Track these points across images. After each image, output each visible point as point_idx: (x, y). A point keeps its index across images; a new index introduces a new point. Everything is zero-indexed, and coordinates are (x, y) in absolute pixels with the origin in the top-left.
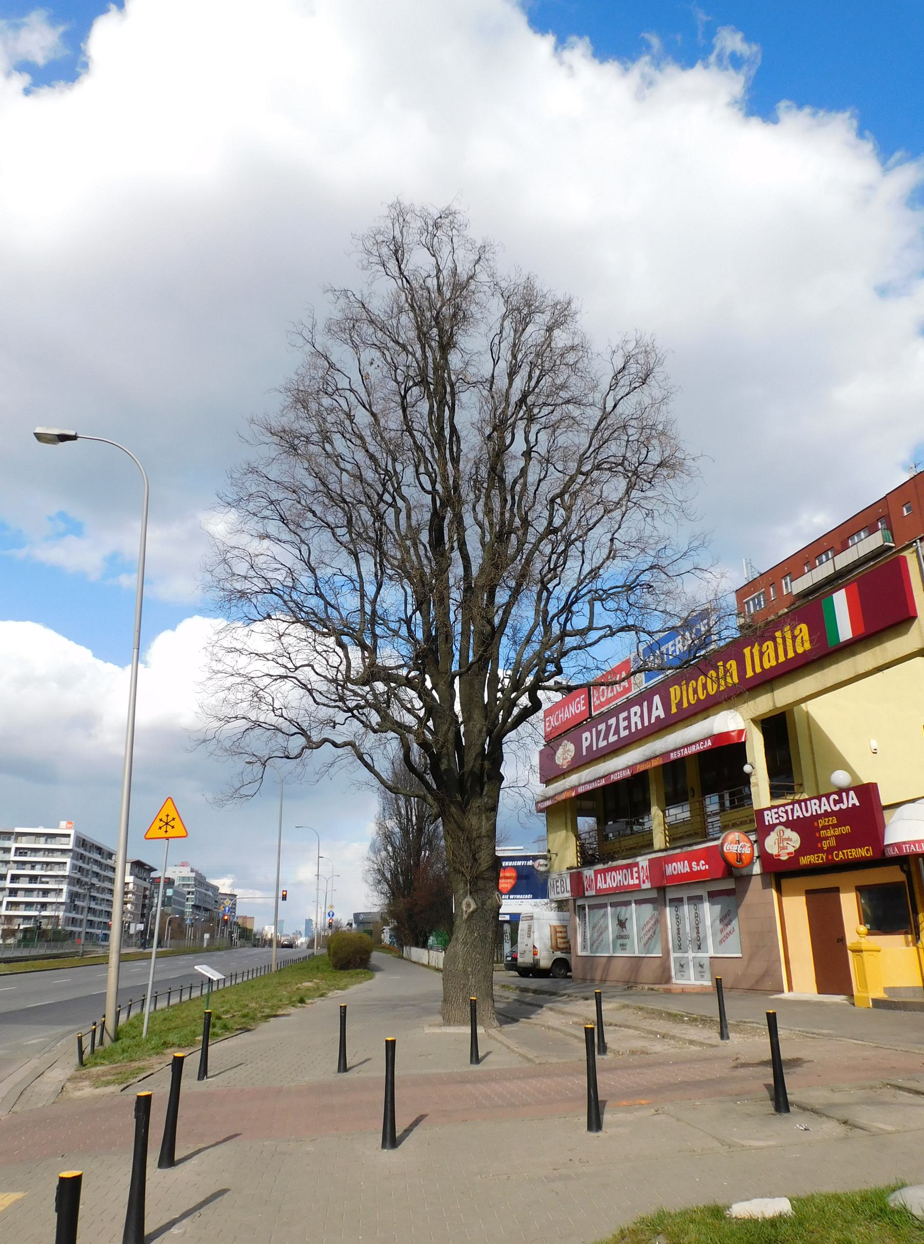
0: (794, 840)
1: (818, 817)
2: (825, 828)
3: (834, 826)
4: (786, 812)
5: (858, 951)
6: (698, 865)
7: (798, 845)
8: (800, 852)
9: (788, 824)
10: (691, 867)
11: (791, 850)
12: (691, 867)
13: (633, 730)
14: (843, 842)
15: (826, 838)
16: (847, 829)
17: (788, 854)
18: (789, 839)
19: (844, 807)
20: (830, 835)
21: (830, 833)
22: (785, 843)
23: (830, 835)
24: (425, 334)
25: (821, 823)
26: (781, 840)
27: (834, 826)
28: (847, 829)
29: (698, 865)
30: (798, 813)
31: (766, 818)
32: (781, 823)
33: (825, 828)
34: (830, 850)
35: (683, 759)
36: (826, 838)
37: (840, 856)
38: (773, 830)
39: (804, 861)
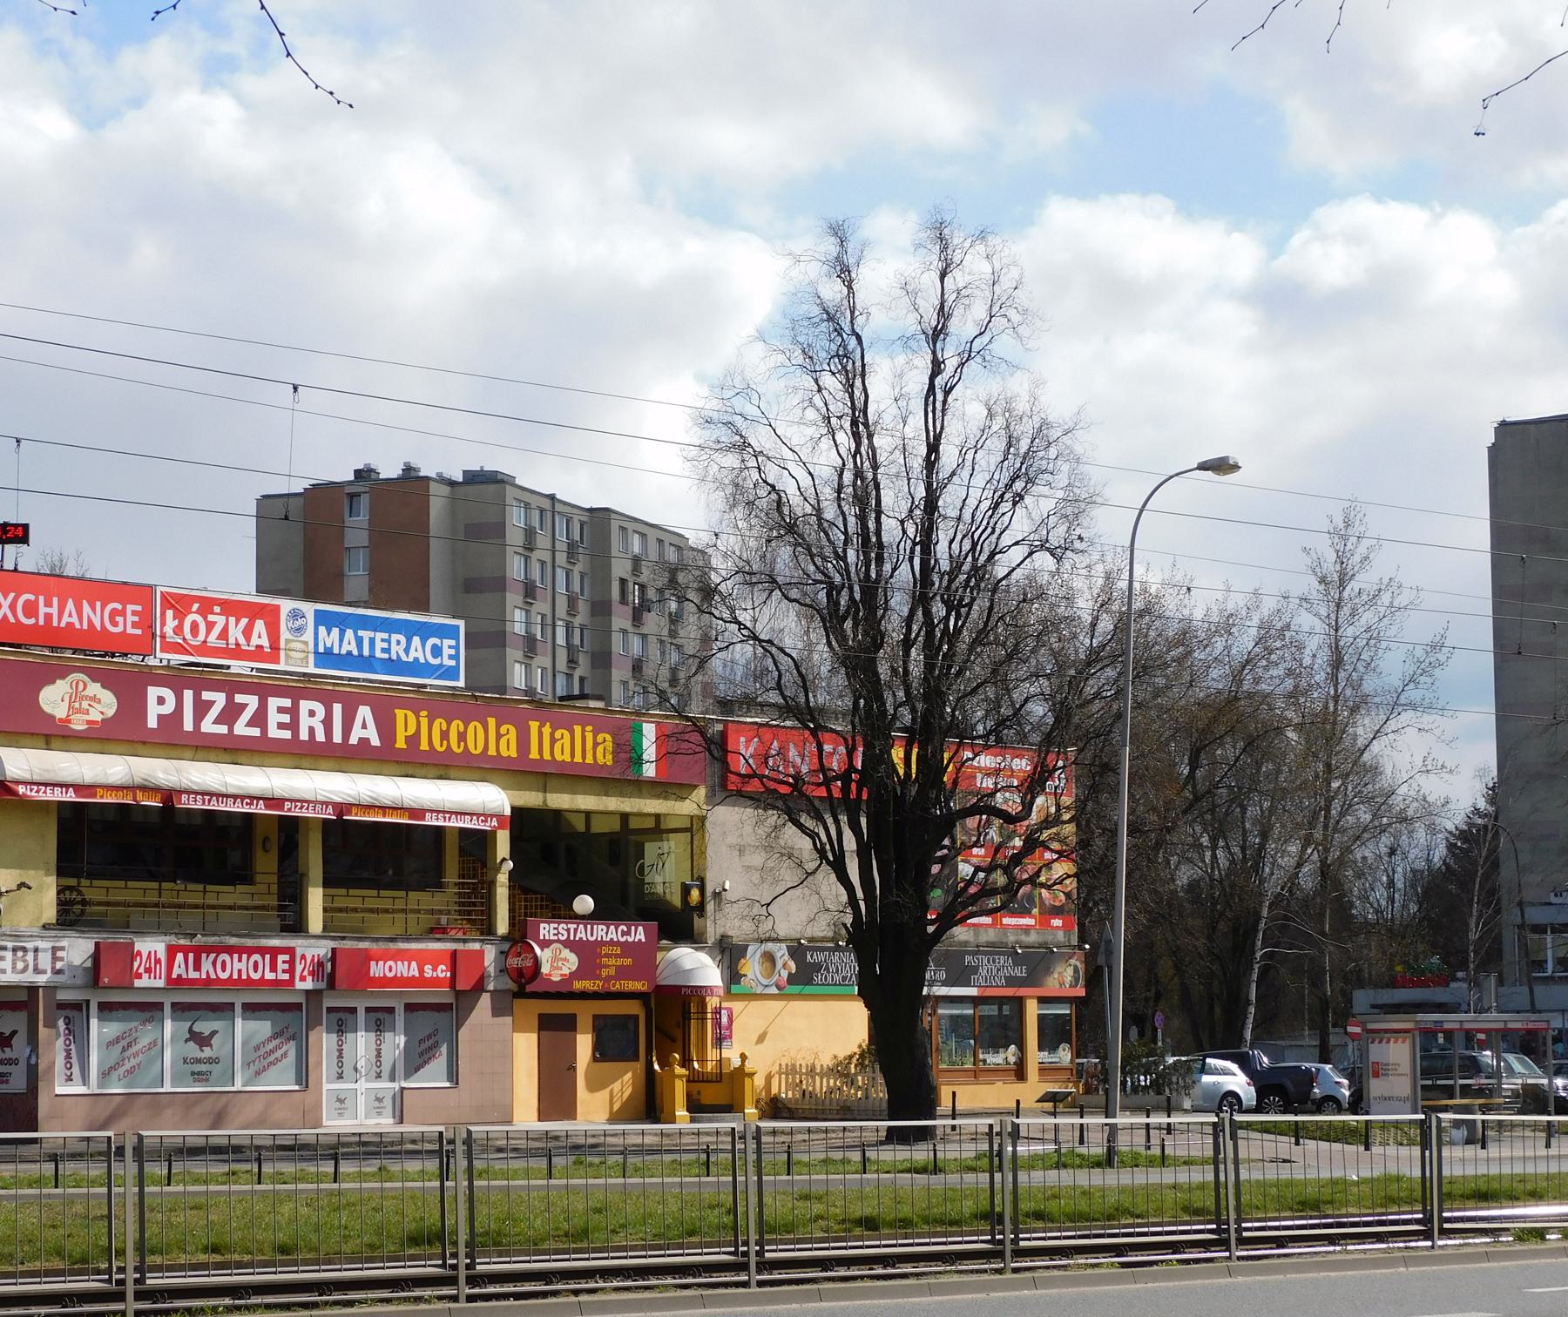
0: (571, 961)
1: (602, 943)
2: (608, 956)
3: (617, 956)
4: (568, 930)
5: (205, 891)
6: (435, 969)
7: (110, 712)
8: (574, 976)
9: (567, 944)
10: (421, 971)
11: (95, 716)
12: (421, 971)
13: (304, 735)
14: (622, 973)
15: (607, 966)
16: (628, 962)
17: (89, 722)
18: (566, 960)
19: (630, 940)
20: (610, 965)
21: (612, 962)
22: (85, 705)
23: (610, 965)
24: (797, 544)
25: (605, 950)
26: (555, 959)
27: (617, 956)
28: (628, 962)
29: (435, 969)
30: (581, 935)
31: (542, 932)
32: (558, 941)
33: (608, 956)
34: (608, 978)
35: (439, 830)
36: (607, 966)
37: (617, 986)
38: (63, 677)
39: (579, 985)
